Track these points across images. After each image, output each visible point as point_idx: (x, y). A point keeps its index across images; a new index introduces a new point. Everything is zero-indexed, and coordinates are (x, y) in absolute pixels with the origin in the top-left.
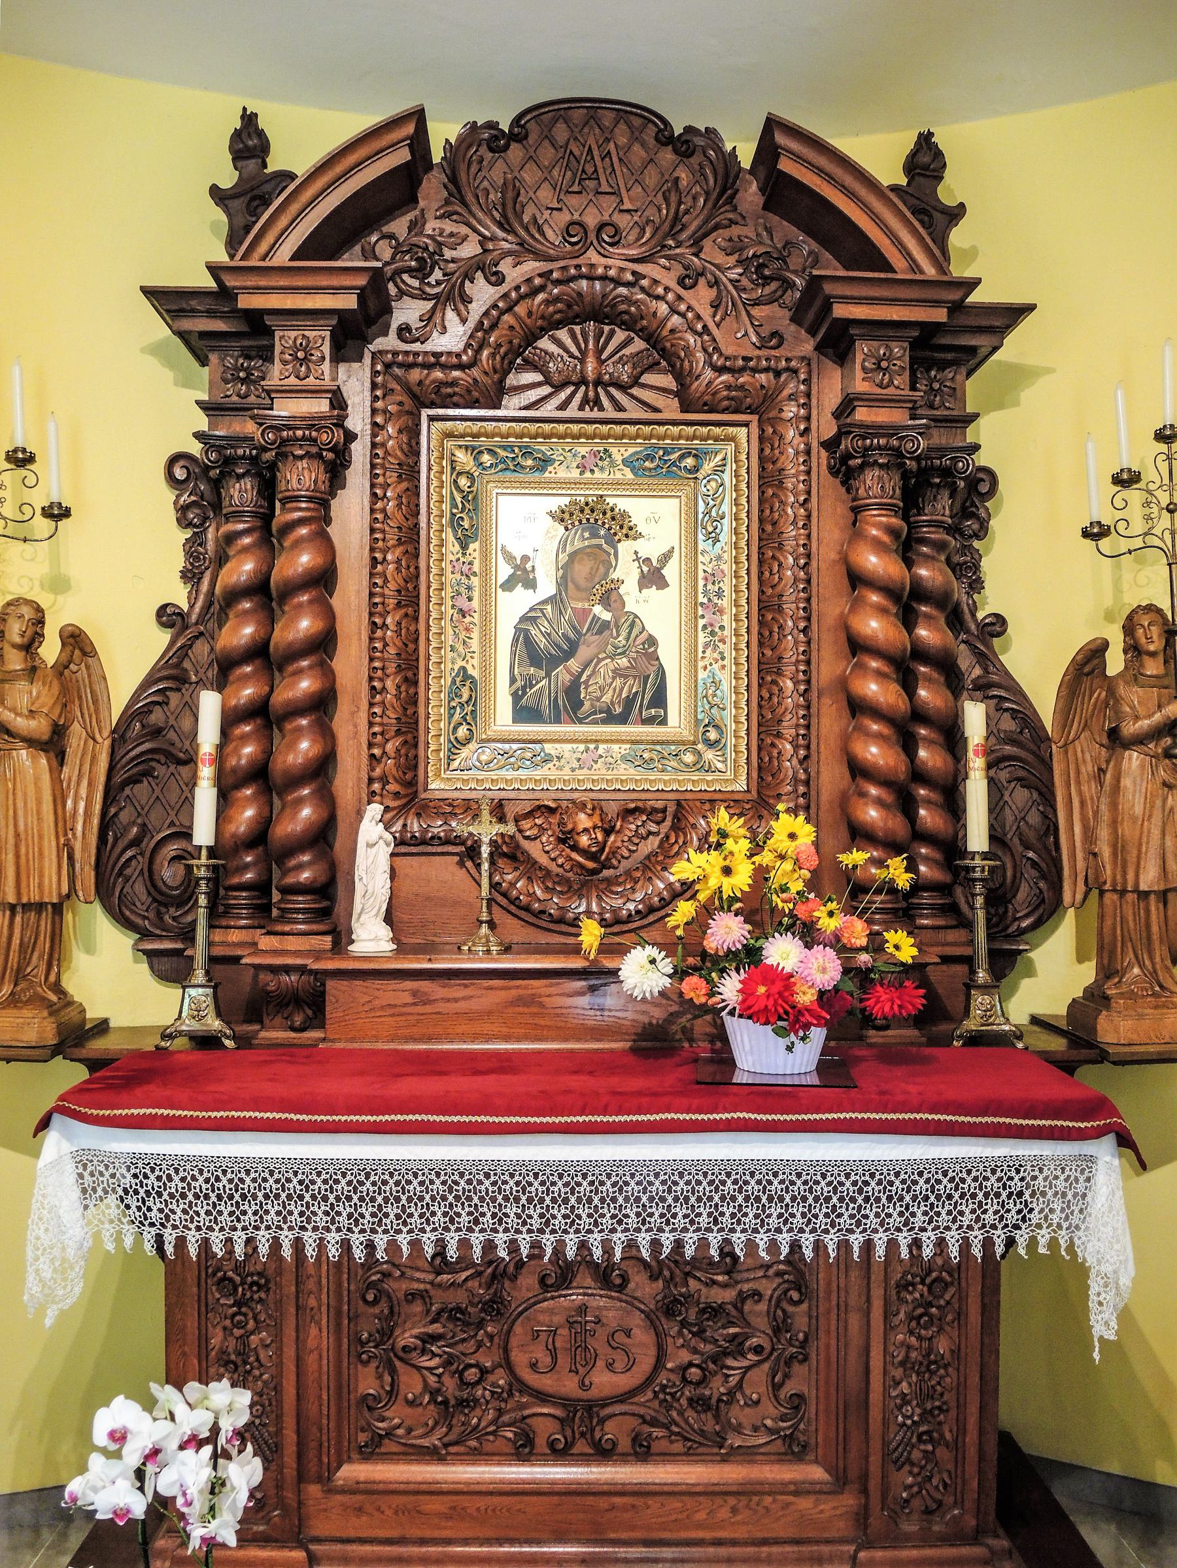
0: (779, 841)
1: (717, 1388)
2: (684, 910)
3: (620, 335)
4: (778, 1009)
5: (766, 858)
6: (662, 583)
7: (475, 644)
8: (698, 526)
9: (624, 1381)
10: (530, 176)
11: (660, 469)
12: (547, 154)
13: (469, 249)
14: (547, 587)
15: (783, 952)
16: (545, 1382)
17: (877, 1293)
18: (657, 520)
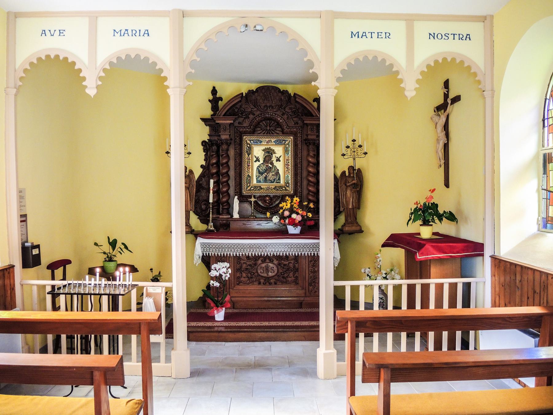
0: (294, 201)
1: (286, 275)
2: (281, 211)
3: (273, 122)
4: (293, 223)
5: (293, 204)
6: (280, 161)
7: (250, 171)
8: (286, 151)
9: (273, 274)
10: (258, 98)
11: (278, 143)
12: (261, 94)
13: (250, 110)
14: (261, 161)
15: (294, 216)
16: (262, 275)
17: (307, 262)
18: (279, 150)
